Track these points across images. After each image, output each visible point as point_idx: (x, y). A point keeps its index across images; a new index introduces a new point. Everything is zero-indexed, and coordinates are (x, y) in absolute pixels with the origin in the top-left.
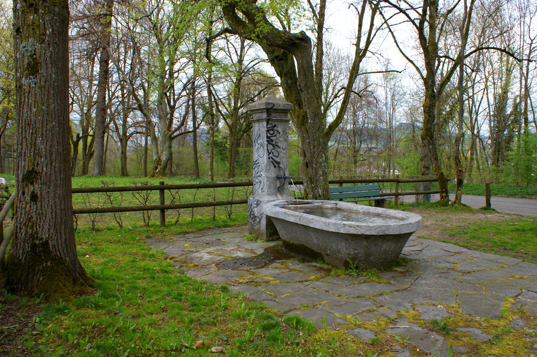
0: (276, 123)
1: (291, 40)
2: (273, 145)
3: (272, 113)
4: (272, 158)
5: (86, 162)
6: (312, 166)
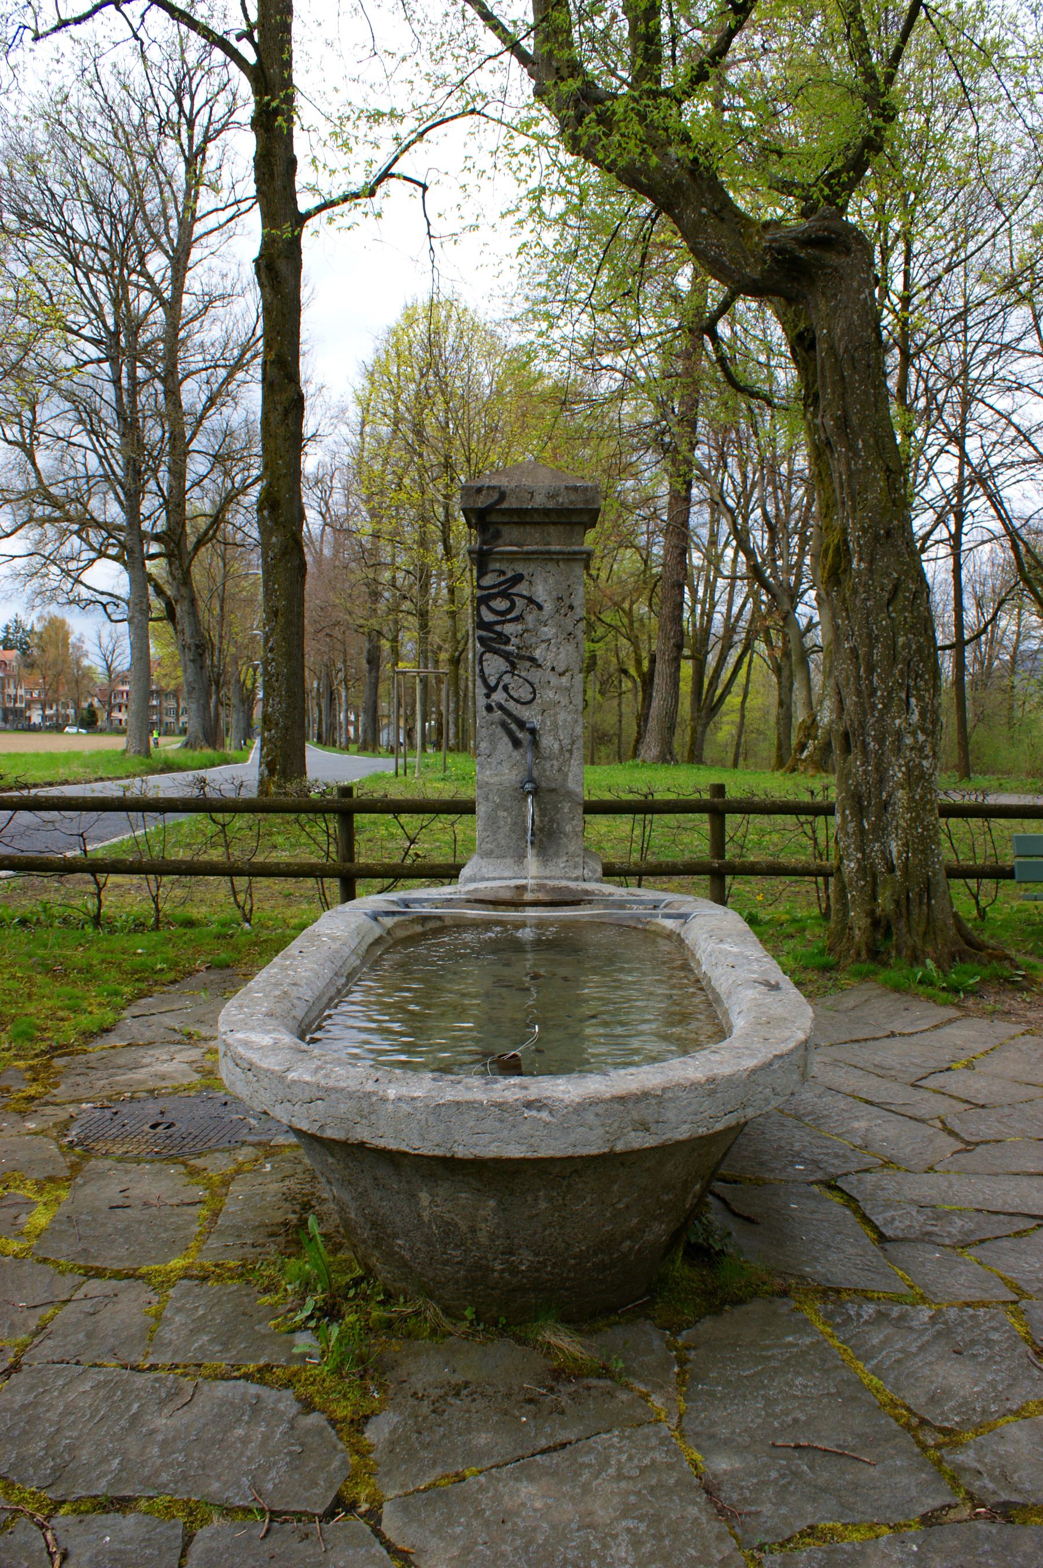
0: (520, 568)
1: (781, 251)
2: (506, 656)
3: (505, 530)
4: (501, 707)
5: (700, 729)
6: (865, 745)
